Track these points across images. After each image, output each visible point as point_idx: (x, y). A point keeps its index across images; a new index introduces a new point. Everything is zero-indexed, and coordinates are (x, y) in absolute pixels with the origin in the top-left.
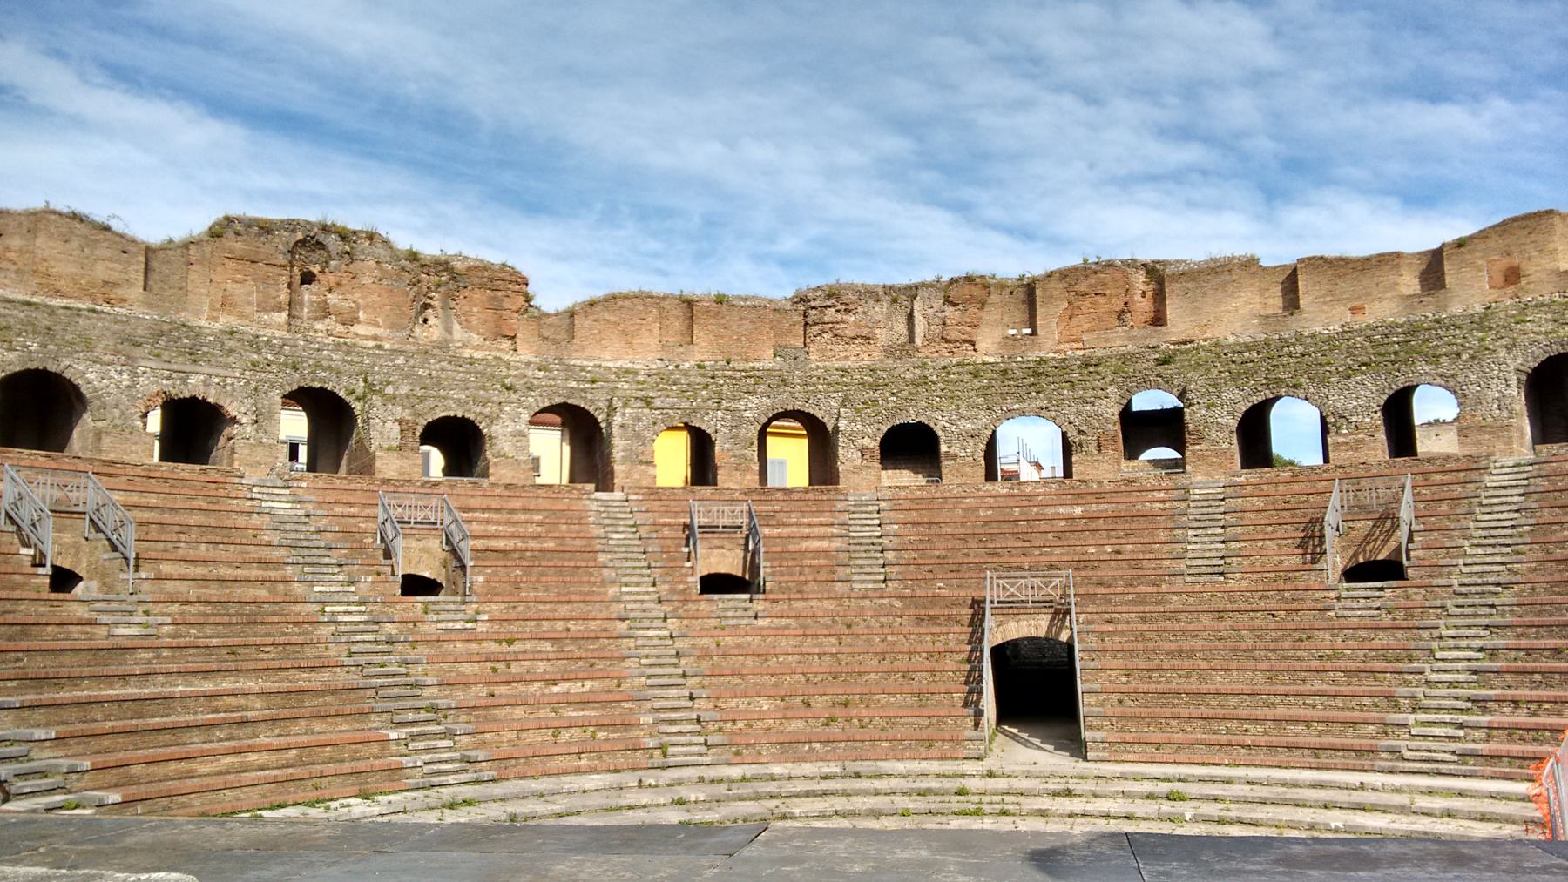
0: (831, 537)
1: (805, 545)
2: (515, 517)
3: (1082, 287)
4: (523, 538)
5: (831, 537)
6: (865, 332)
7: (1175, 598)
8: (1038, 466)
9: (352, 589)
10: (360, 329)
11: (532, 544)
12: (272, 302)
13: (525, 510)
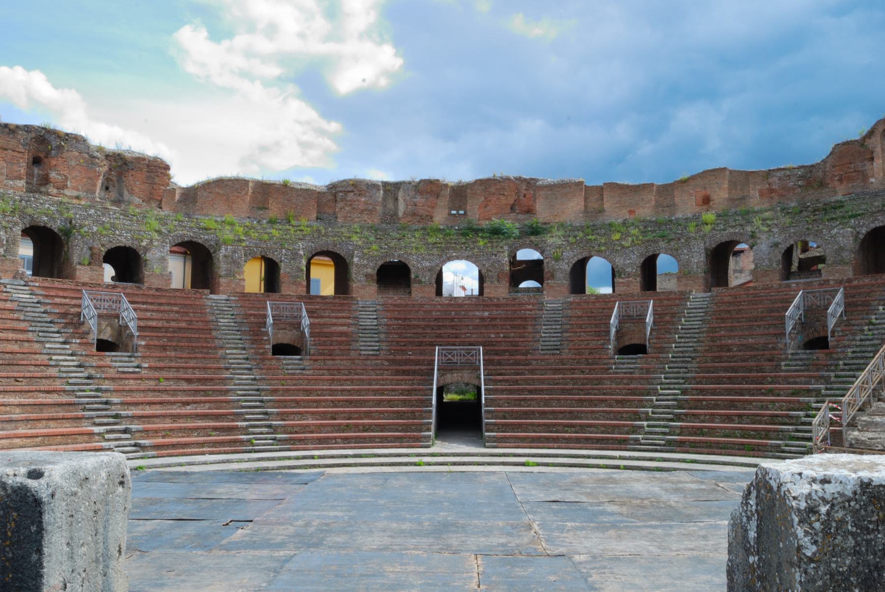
0: (349, 325)
1: (333, 329)
3: (492, 190)
4: (168, 321)
5: (349, 325)
6: (370, 207)
7: (534, 362)
8: (464, 288)
9: (68, 346)
10: (67, 192)
11: (173, 324)
12: (15, 174)
13: (169, 304)
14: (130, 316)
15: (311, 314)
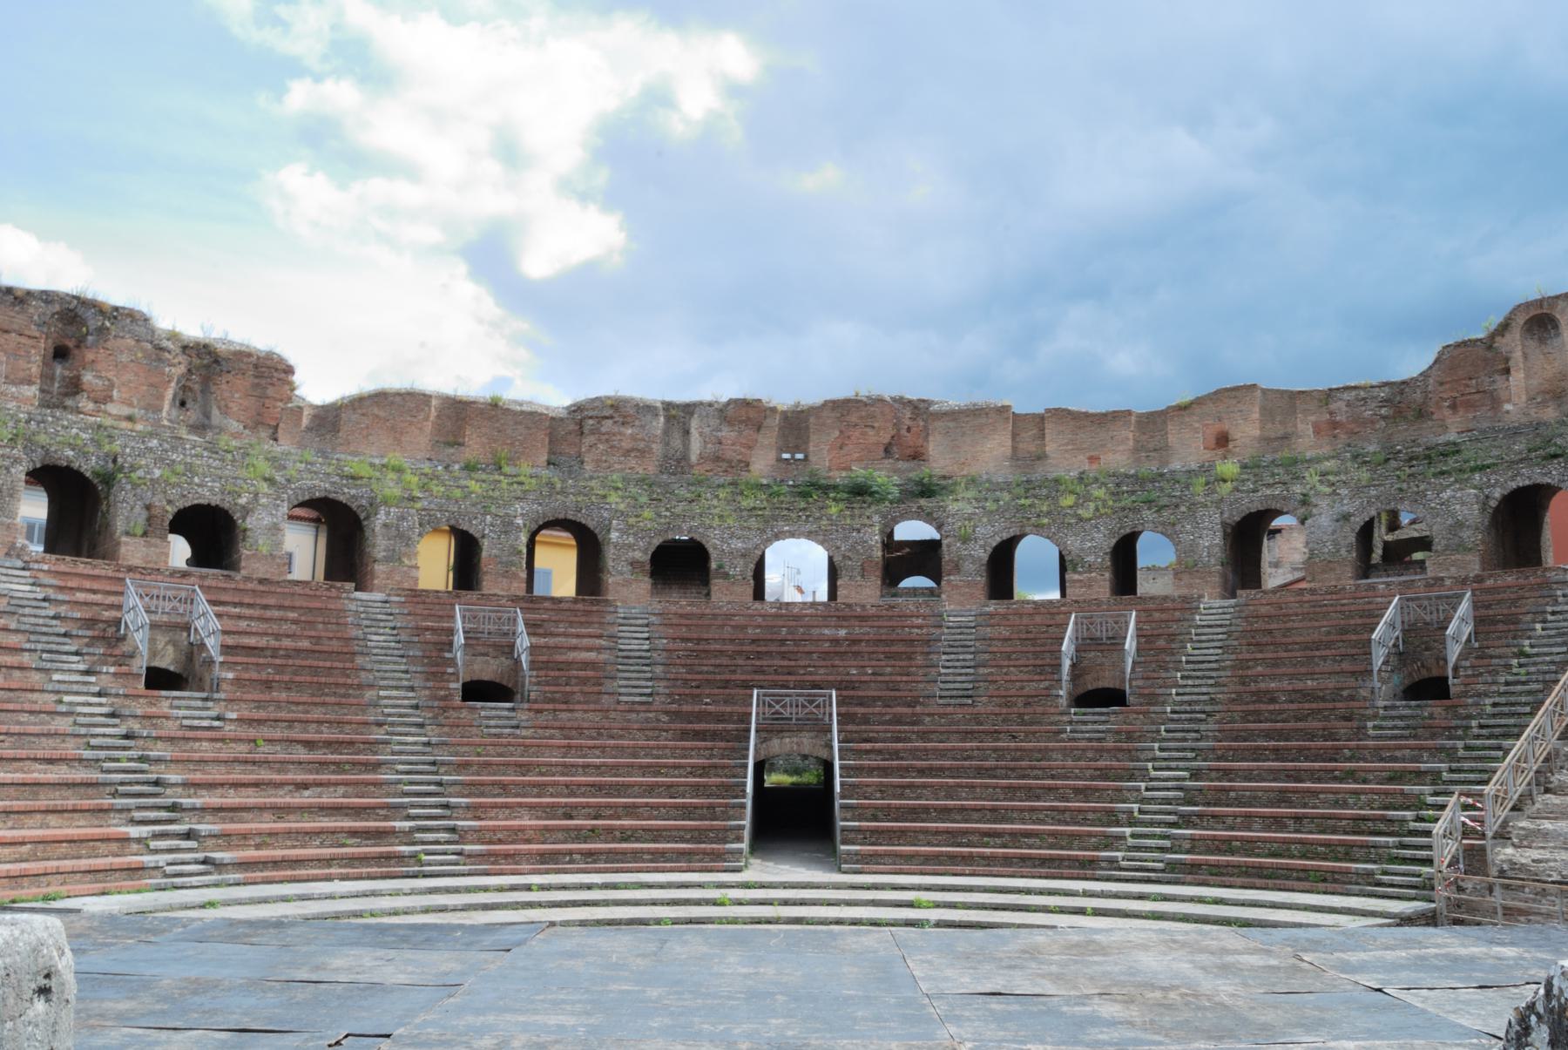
0: (599, 649)
1: (572, 655)
2: (268, 614)
3: (853, 419)
4: (277, 636)
5: (599, 649)
6: (642, 445)
7: (928, 719)
9: (93, 679)
10: (112, 408)
11: (287, 643)
12: (21, 375)
13: (281, 607)
14: (209, 627)
15: (533, 628)
